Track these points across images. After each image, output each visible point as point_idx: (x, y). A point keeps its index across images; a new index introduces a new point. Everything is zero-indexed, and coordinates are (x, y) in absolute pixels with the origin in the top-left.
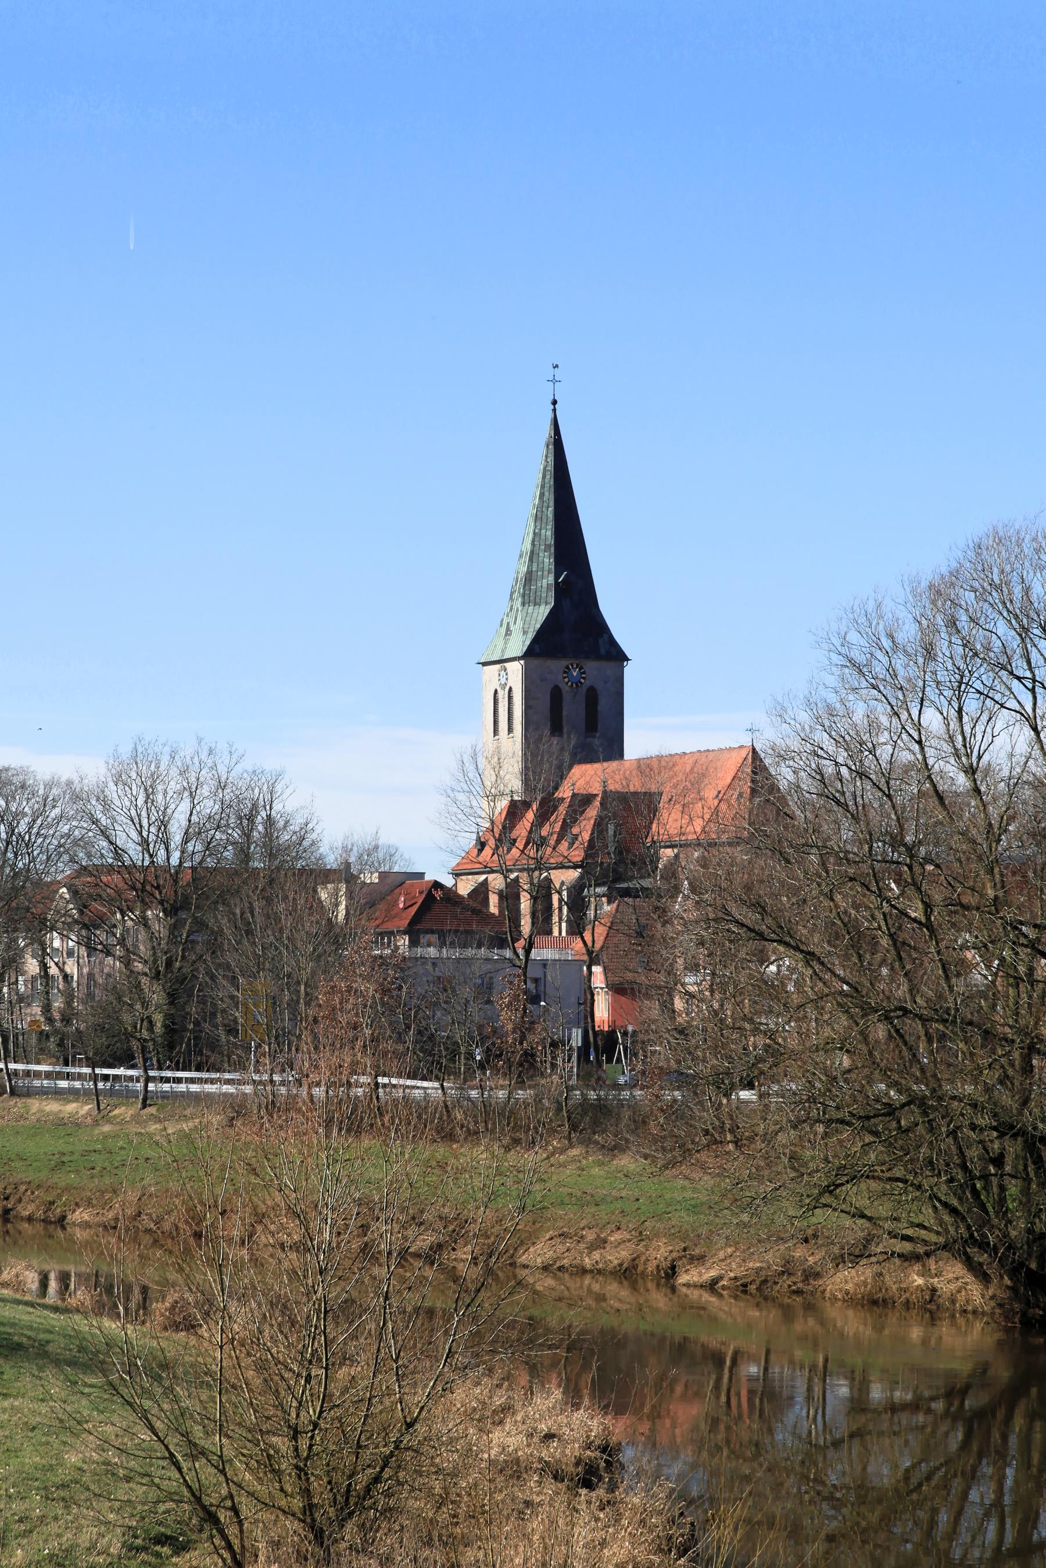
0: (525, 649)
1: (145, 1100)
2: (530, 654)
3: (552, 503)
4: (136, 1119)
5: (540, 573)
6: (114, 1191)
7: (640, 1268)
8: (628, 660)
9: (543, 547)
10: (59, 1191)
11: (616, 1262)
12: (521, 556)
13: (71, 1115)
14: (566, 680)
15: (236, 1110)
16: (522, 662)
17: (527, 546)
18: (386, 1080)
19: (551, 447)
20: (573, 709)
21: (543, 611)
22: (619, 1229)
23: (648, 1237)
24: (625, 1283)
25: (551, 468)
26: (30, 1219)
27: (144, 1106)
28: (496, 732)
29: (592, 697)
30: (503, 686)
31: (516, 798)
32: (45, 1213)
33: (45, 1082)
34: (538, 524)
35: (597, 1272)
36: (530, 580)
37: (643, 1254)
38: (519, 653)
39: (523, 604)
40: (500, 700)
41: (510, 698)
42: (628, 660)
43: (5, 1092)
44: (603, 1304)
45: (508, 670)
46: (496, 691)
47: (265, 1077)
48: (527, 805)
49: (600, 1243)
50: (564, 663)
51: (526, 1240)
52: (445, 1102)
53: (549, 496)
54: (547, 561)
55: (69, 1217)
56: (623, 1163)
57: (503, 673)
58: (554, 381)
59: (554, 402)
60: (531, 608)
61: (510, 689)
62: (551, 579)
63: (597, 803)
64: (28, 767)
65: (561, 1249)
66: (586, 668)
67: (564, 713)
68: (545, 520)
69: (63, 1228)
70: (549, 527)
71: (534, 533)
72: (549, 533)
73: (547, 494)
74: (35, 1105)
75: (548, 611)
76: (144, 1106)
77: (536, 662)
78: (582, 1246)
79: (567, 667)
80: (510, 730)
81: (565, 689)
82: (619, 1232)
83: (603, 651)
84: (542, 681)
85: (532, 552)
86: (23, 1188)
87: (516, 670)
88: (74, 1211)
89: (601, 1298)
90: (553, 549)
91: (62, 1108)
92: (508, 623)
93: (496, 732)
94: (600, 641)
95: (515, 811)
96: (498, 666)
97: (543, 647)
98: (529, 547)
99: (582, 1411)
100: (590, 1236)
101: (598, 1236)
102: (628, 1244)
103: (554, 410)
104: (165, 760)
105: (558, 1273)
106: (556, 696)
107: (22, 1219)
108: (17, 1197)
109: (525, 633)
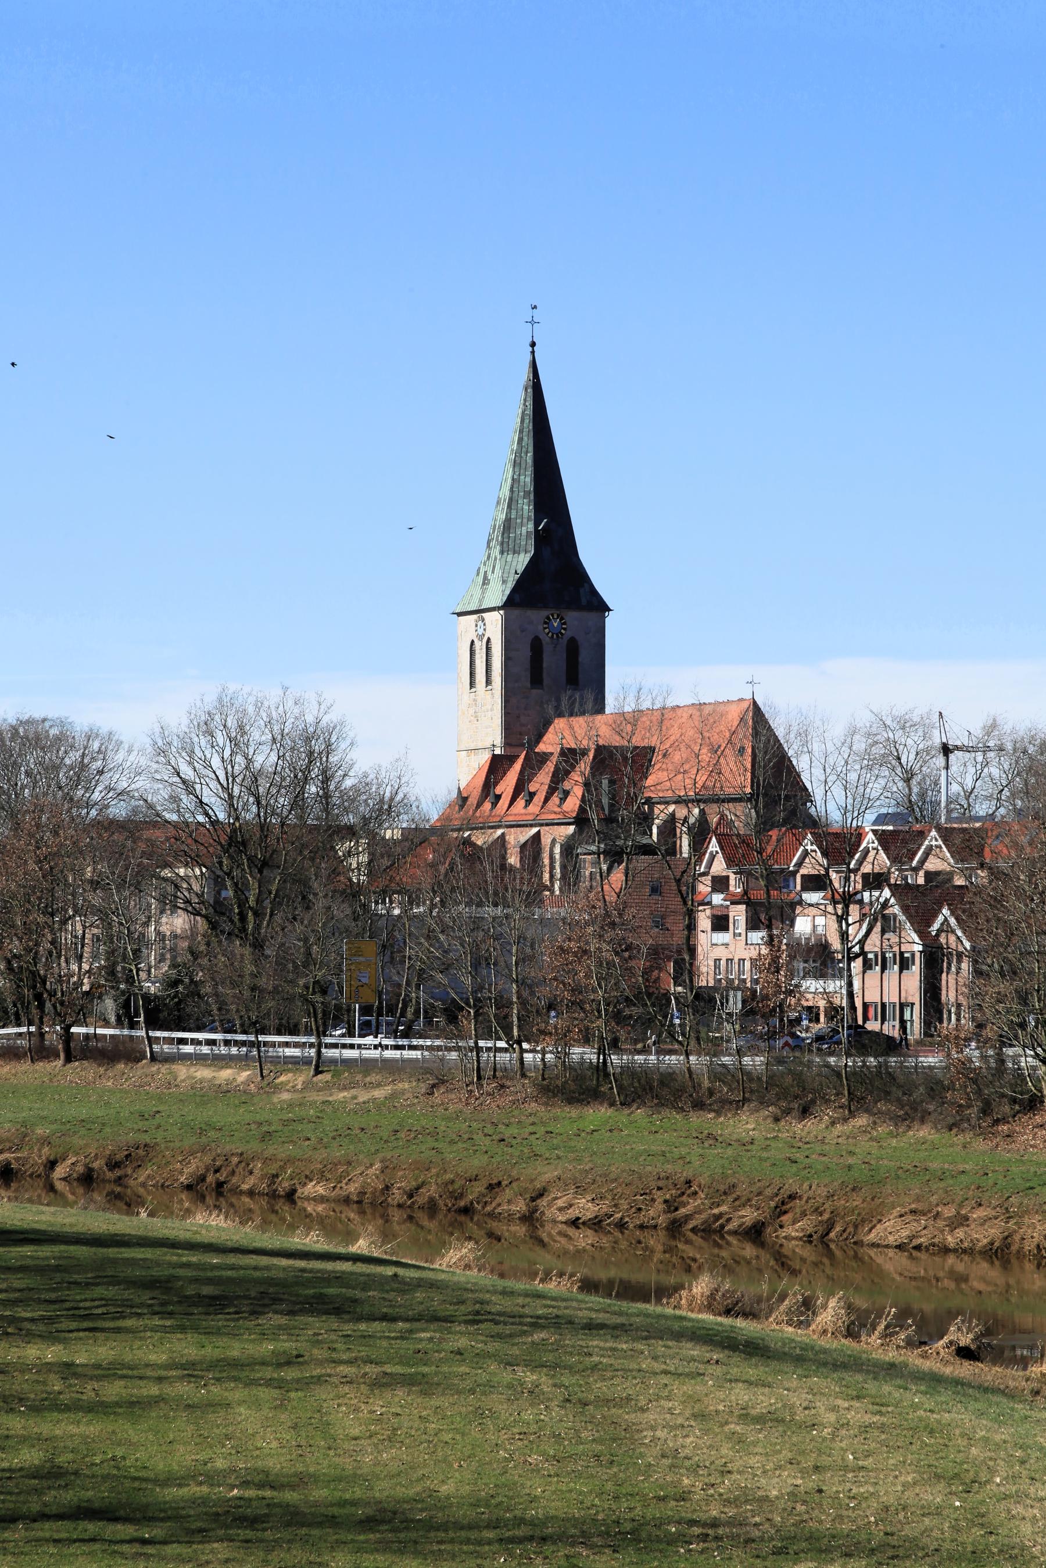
0: (505, 599)
1: (317, 1066)
2: (510, 604)
3: (531, 449)
4: (307, 1086)
5: (519, 521)
6: (349, 1163)
7: (1014, 1248)
8: (609, 610)
9: (522, 494)
10: (282, 1163)
11: (985, 1241)
12: (498, 503)
13: (228, 1082)
14: (547, 630)
15: (437, 1078)
16: (502, 612)
17: (506, 492)
18: (490, 1044)
19: (530, 390)
20: (553, 661)
21: (522, 561)
22: (980, 1205)
23: (1016, 1214)
24: (997, 1263)
25: (529, 411)
26: (251, 1193)
27: (318, 1072)
28: (472, 684)
29: (573, 649)
30: (481, 637)
31: (498, 752)
32: (268, 1186)
33: (165, 1046)
34: (517, 469)
35: (960, 1251)
36: (509, 528)
37: (1015, 1231)
38: (499, 603)
39: (502, 552)
40: (477, 652)
41: (488, 649)
42: (609, 610)
43: (145, 1057)
44: (963, 1286)
45: (486, 621)
46: (473, 642)
47: (471, 1043)
48: (511, 759)
49: (961, 1221)
50: (545, 613)
51: (872, 1217)
52: (689, 1069)
53: (529, 442)
54: (527, 508)
55: (300, 1191)
56: (921, 1134)
57: (480, 623)
58: (532, 322)
59: (533, 344)
60: (510, 557)
61: (489, 640)
62: (531, 526)
63: (591, 754)
64: (67, 718)
65: (914, 1226)
66: (567, 619)
67: (545, 665)
68: (523, 466)
69: (293, 1202)
70: (529, 473)
71: (513, 479)
72: (528, 479)
73: (525, 438)
74: (182, 1071)
75: (527, 560)
76: (318, 1072)
77: (516, 612)
78: (941, 1223)
79: (548, 618)
80: (488, 682)
81: (546, 640)
82: (981, 1208)
83: (584, 601)
84: (522, 631)
85: (511, 499)
86: (235, 1160)
87: (495, 622)
88: (305, 1184)
89: (961, 1279)
90: (532, 497)
91: (214, 1074)
92: (486, 572)
93: (472, 684)
94: (582, 591)
95: (497, 766)
96: (475, 617)
97: (523, 597)
98: (507, 494)
99: (550, 1382)
100: (949, 1212)
101: (958, 1213)
102: (996, 1222)
103: (533, 352)
104: (251, 709)
105: (915, 1253)
106: (537, 646)
107: (242, 1192)
108: (230, 1169)
109: (504, 582)
